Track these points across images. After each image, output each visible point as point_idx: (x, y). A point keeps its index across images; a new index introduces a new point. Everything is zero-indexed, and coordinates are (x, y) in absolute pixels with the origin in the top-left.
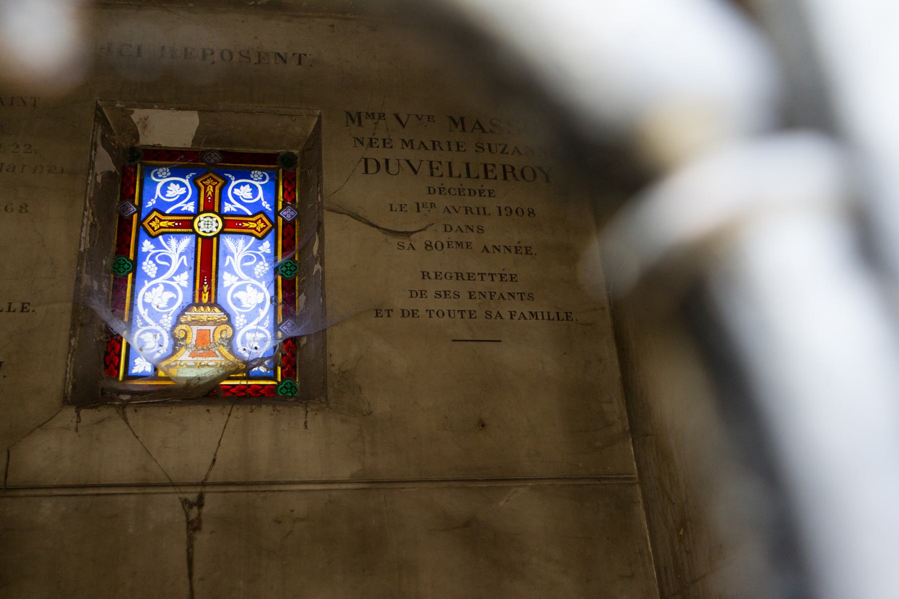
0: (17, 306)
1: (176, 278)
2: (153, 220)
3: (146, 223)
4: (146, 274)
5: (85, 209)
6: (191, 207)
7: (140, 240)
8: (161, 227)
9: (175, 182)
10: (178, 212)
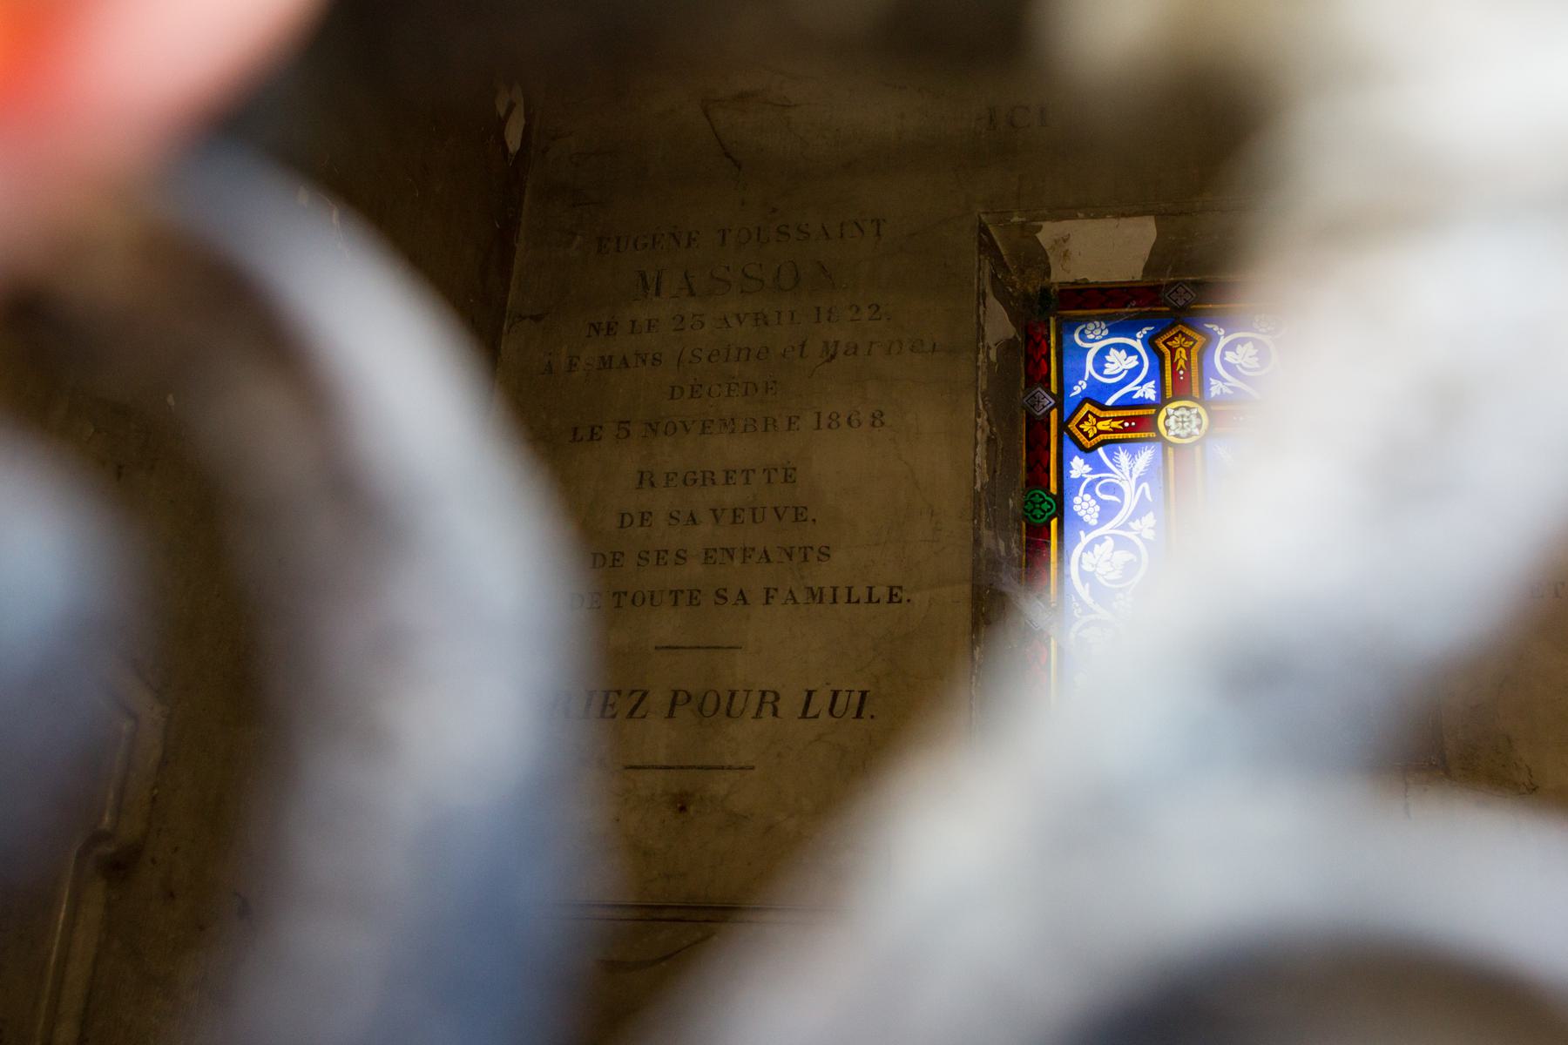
0: (881, 592)
1: (1135, 525)
2: (1085, 418)
3: (1072, 426)
4: (1081, 519)
5: (978, 415)
6: (1149, 392)
7: (1065, 457)
8: (1100, 432)
9: (1118, 347)
10: (1125, 402)
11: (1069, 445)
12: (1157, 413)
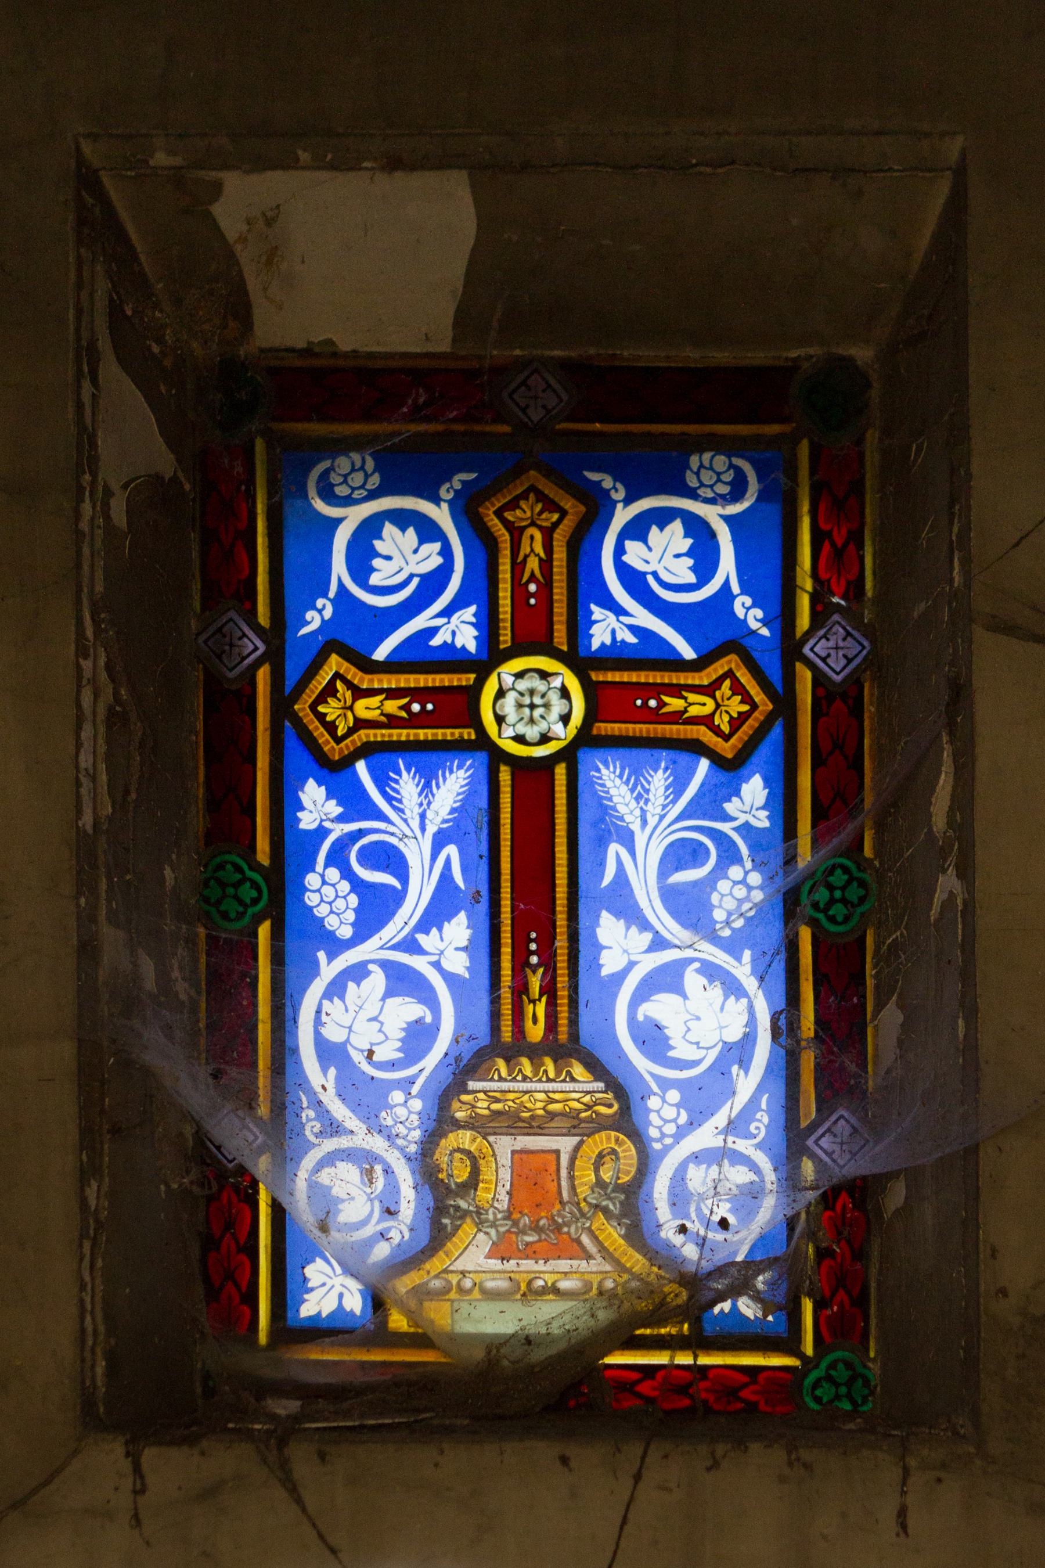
1: (428, 941)
2: (330, 690)
3: (302, 707)
5: (82, 651)
6: (463, 633)
8: (361, 724)
9: (402, 519)
10: (407, 656)
11: (296, 755)
12: (480, 682)
